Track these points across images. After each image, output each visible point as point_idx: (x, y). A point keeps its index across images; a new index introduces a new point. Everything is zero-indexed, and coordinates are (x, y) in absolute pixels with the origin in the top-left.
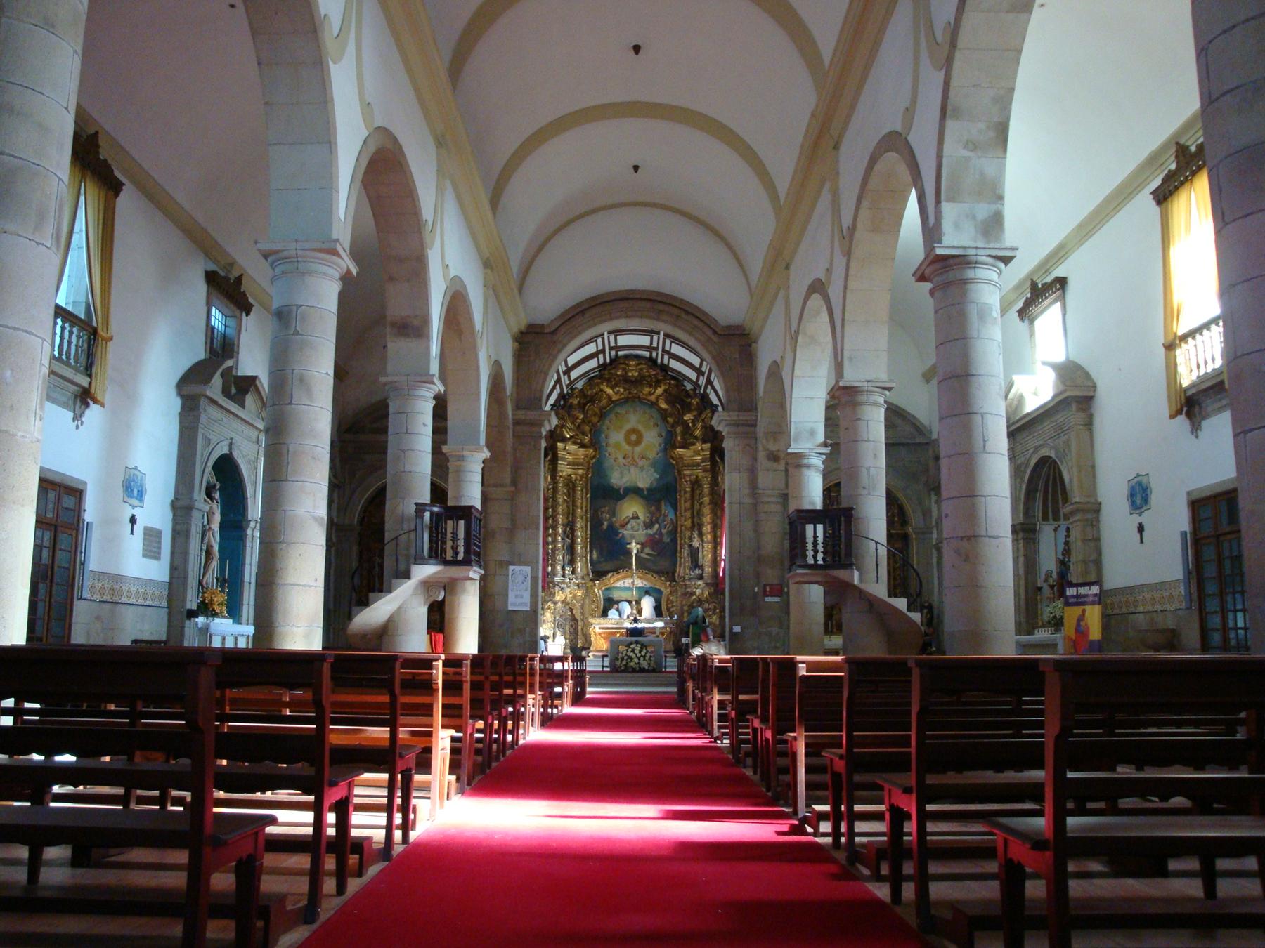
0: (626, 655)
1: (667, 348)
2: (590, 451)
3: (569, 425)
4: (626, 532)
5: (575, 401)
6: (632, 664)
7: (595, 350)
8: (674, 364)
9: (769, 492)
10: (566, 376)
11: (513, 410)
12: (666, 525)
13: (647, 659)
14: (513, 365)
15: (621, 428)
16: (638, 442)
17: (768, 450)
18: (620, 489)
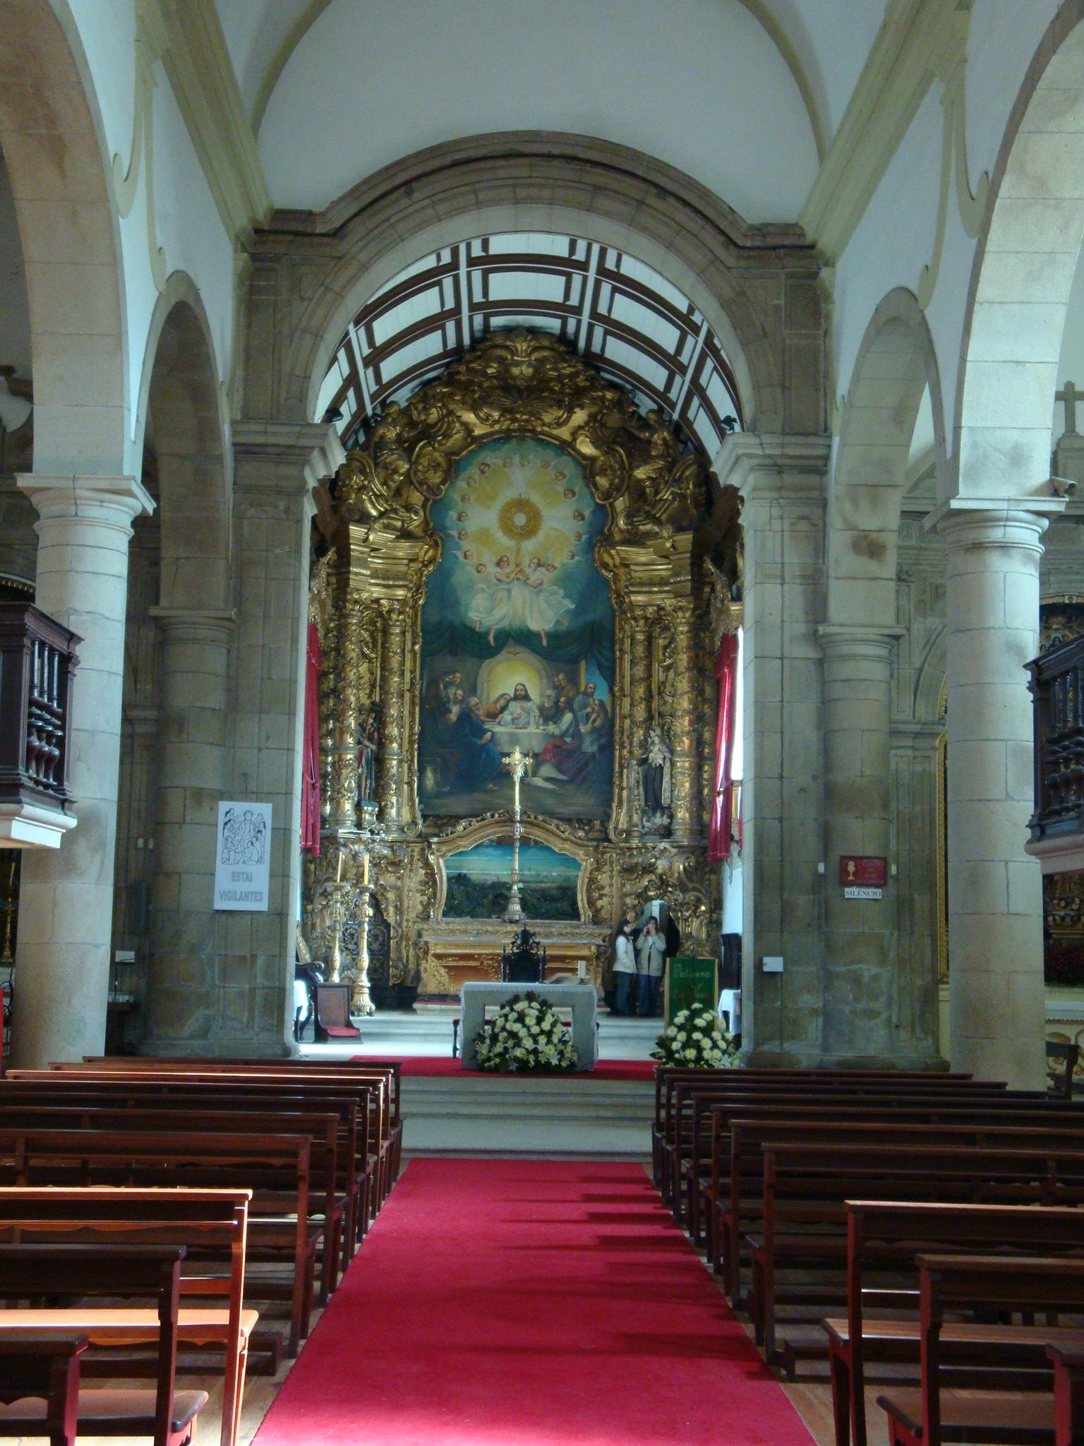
0: (504, 1029)
1: (603, 309)
2: (424, 551)
3: (377, 486)
4: (500, 729)
5: (392, 433)
6: (519, 1052)
7: (438, 310)
8: (618, 351)
9: (859, 632)
10: (370, 370)
11: (234, 423)
12: (588, 716)
13: (555, 1039)
14: (237, 312)
15: (492, 498)
16: (529, 531)
17: (855, 528)
18: (487, 633)
